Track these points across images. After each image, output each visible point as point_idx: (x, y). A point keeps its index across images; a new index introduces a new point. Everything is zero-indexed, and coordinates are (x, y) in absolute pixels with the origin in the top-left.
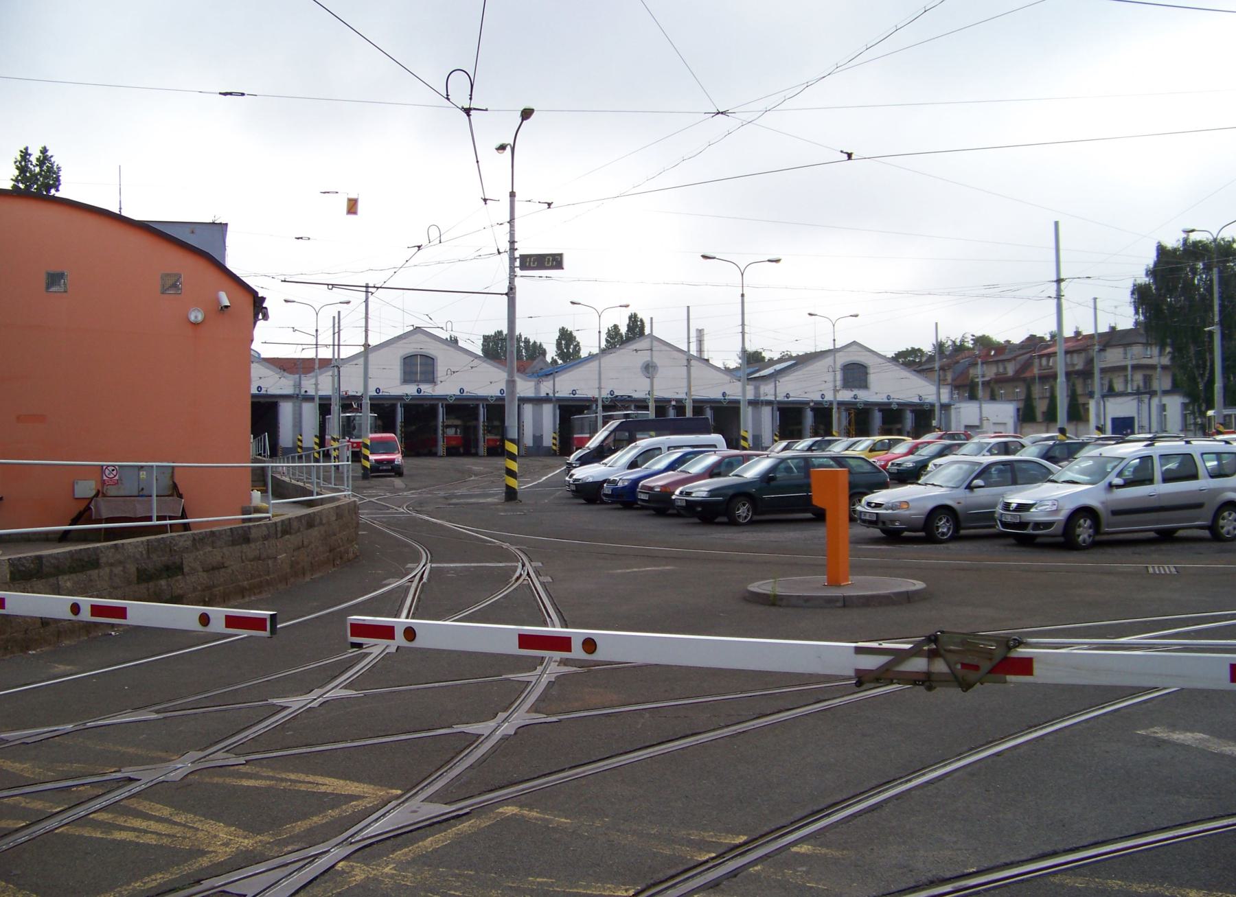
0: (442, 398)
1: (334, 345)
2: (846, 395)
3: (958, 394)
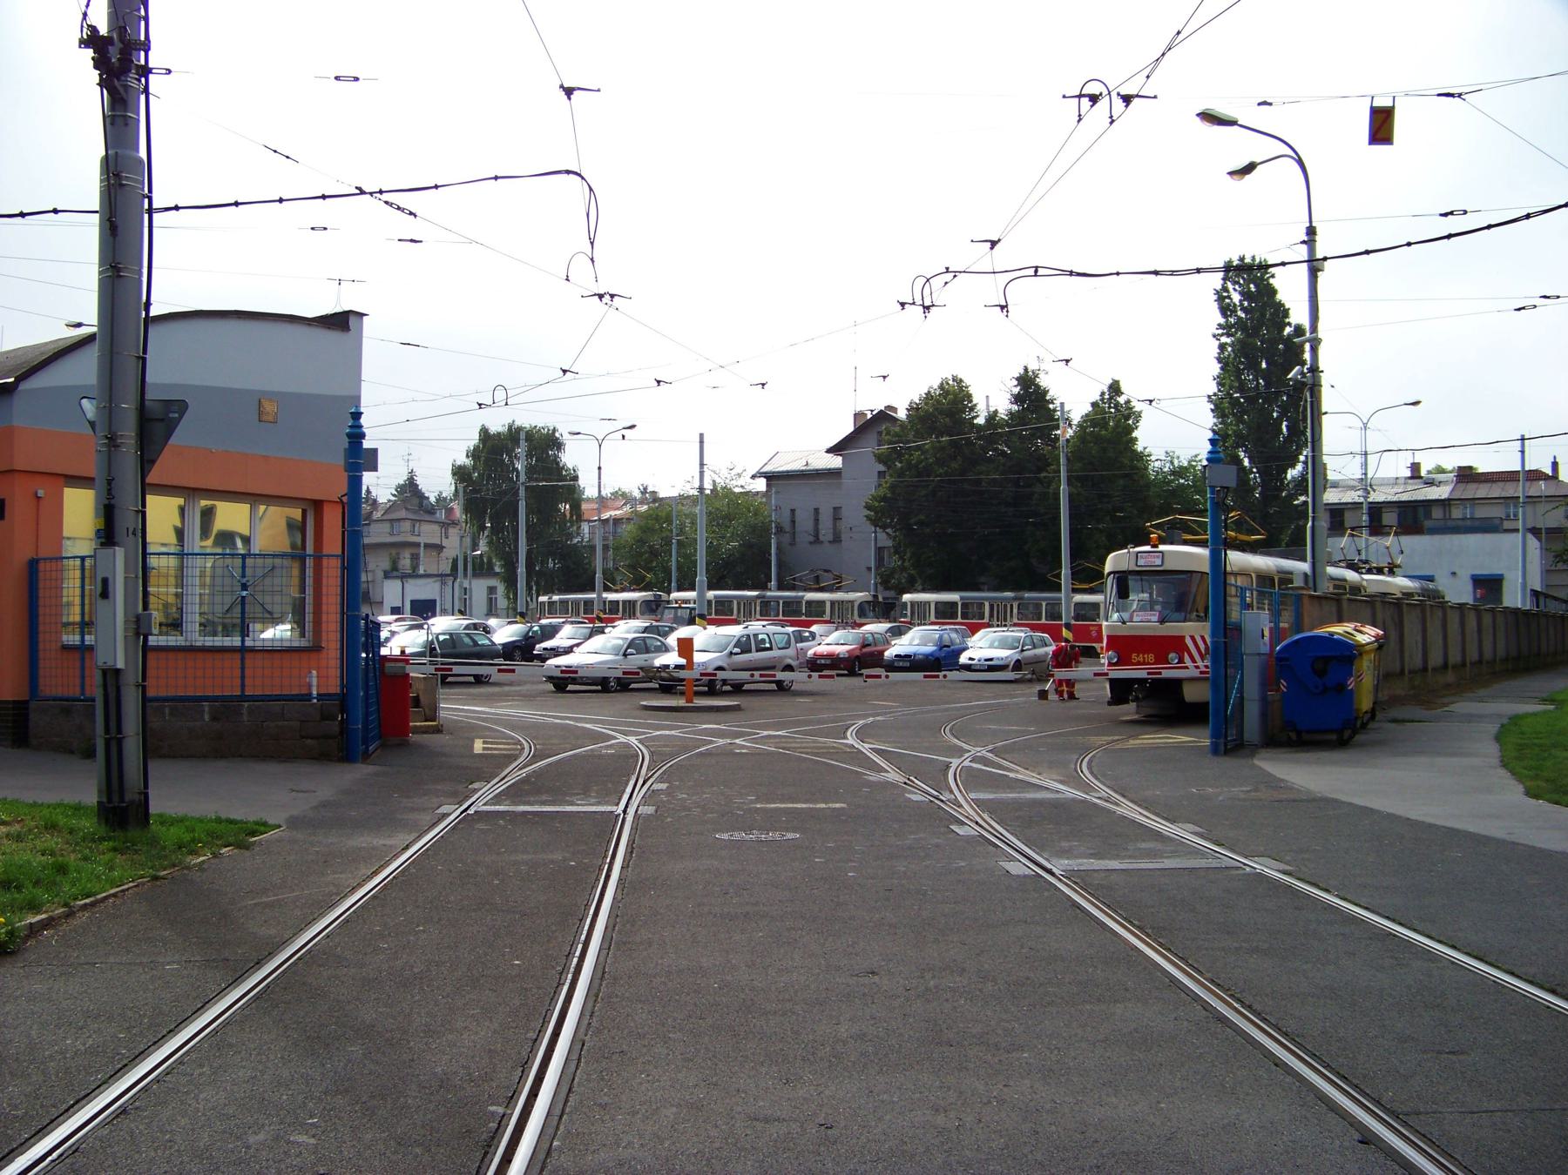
1: (328, 622)
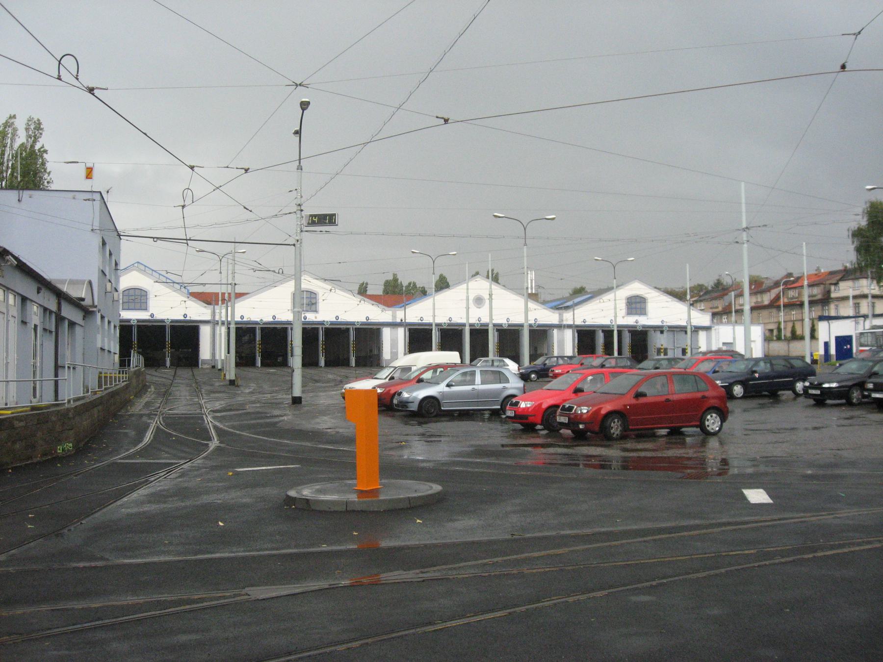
0: (322, 323)
2: (630, 321)
3: (727, 318)
